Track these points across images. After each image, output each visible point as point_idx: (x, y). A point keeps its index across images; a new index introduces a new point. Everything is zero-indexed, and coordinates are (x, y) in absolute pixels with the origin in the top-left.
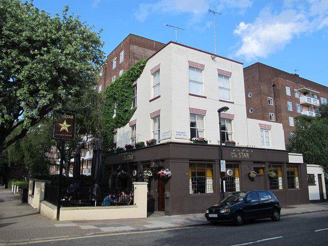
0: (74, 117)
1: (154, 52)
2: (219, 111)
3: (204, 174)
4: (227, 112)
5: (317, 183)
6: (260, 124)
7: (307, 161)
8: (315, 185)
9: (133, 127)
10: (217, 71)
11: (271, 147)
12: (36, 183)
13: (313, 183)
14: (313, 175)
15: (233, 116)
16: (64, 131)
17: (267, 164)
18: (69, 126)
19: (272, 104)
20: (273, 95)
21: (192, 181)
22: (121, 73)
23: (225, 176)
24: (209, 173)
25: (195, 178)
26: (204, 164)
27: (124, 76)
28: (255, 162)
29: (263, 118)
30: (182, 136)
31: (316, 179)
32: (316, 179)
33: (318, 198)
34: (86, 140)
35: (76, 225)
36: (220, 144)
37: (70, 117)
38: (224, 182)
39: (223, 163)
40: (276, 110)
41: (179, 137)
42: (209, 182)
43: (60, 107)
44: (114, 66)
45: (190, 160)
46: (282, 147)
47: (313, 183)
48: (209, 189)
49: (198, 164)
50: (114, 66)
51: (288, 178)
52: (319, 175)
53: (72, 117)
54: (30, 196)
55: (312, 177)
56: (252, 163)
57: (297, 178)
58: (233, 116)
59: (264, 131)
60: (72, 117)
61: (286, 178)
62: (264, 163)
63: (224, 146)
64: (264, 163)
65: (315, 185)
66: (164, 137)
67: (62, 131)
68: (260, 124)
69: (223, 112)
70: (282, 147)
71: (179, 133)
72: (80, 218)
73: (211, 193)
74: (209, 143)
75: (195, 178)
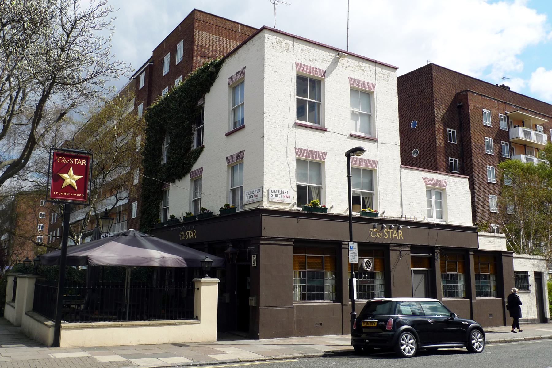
0: (87, 163)
1: (238, 44)
2: (348, 155)
4: (363, 156)
5: (533, 288)
6: (425, 179)
7: (513, 247)
9: (197, 181)
10: (348, 83)
12: (19, 280)
14: (526, 273)
15: (375, 163)
18: (78, 177)
22: (178, 82)
27: (181, 89)
29: (433, 167)
30: (282, 199)
31: (531, 280)
32: (531, 280)
34: (83, 76)
35: (89, 355)
36: (347, 213)
38: (355, 280)
39: (353, 247)
43: (21, 18)
44: (166, 69)
47: (525, 288)
50: (166, 69)
53: (84, 162)
54: (8, 304)
55: (522, 277)
58: (375, 163)
60: (84, 162)
63: (356, 219)
66: (249, 200)
67: (66, 187)
68: (425, 179)
69: (355, 156)
71: (277, 193)
72: (94, 344)
73: (352, 300)
74: (511, 90)
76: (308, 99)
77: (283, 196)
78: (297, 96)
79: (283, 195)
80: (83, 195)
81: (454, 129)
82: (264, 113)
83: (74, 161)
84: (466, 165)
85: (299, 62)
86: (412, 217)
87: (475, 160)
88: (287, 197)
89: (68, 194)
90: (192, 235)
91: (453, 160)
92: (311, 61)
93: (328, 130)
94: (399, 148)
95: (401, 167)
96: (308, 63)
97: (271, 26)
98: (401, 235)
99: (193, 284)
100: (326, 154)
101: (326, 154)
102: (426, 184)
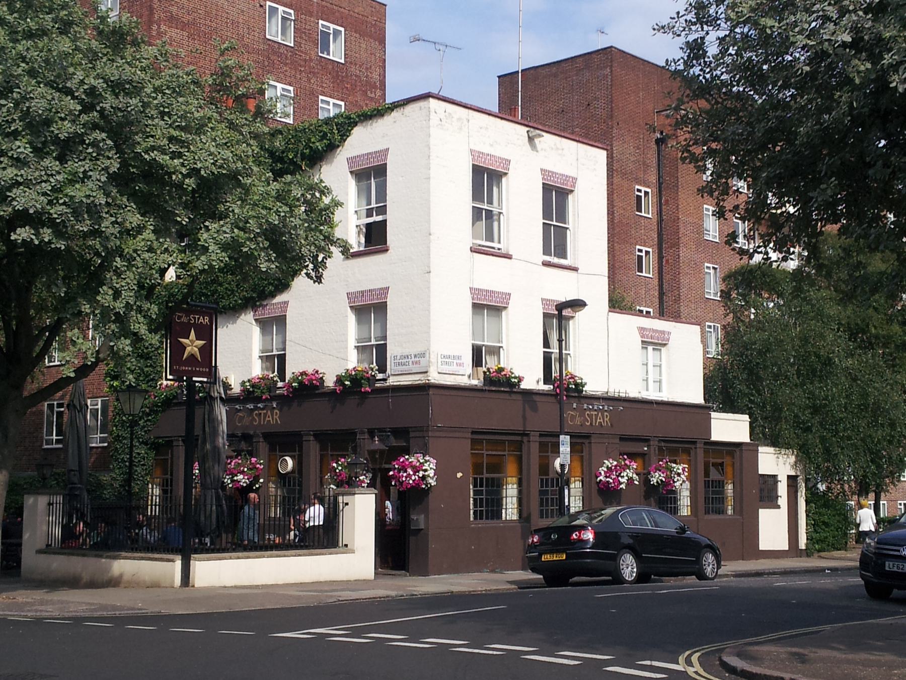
3: (497, 467)
5: (783, 501)
6: (641, 330)
8: (779, 507)
11: (666, 395)
13: (771, 501)
14: (775, 476)
16: (192, 356)
17: (654, 443)
19: (649, 212)
20: (653, 178)
21: (475, 486)
23: (551, 475)
24: (511, 468)
25: (481, 479)
26: (503, 442)
28: (623, 439)
30: (453, 368)
31: (782, 489)
32: (782, 489)
33: (783, 544)
37: (201, 320)
40: (660, 235)
41: (446, 369)
42: (511, 492)
45: (541, 435)
46: (696, 396)
48: (510, 511)
49: (488, 441)
51: (707, 484)
52: (792, 480)
56: (617, 441)
57: (730, 487)
59: (650, 348)
61: (701, 485)
62: (645, 440)
64: (645, 440)
65: (779, 507)
68: (641, 330)
70: (696, 396)
71: (447, 359)
75: (481, 479)
76: (485, 207)
77: (455, 364)
78: (544, 254)
79: (455, 361)
80: (207, 370)
81: (648, 187)
82: (430, 234)
83: (195, 318)
84: (667, 261)
85: (477, 148)
86: (617, 391)
87: (684, 253)
88: (460, 365)
89: (190, 369)
90: (271, 419)
91: (644, 252)
92: (492, 145)
93: (513, 257)
94: (606, 279)
95: (610, 311)
96: (486, 150)
97: (435, 91)
98: (608, 419)
99: (788, 446)
100: (510, 295)
101: (510, 295)
102: (642, 337)
